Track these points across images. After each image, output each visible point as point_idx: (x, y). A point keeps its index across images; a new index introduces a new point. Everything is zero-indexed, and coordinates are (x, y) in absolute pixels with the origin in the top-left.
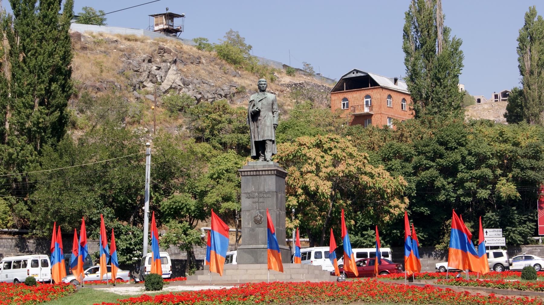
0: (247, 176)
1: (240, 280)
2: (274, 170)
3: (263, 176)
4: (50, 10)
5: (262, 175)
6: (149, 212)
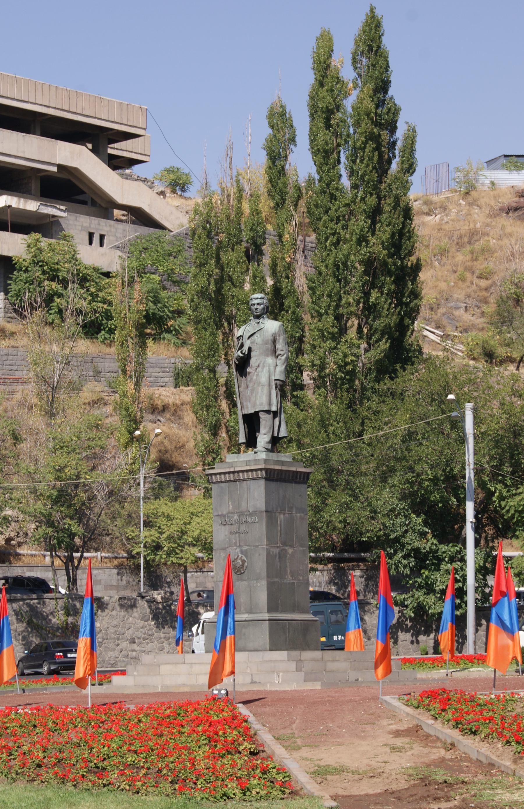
0: (221, 482)
1: (162, 687)
2: (261, 470)
3: (245, 482)
4: (358, 161)
5: (244, 480)
6: (474, 520)
